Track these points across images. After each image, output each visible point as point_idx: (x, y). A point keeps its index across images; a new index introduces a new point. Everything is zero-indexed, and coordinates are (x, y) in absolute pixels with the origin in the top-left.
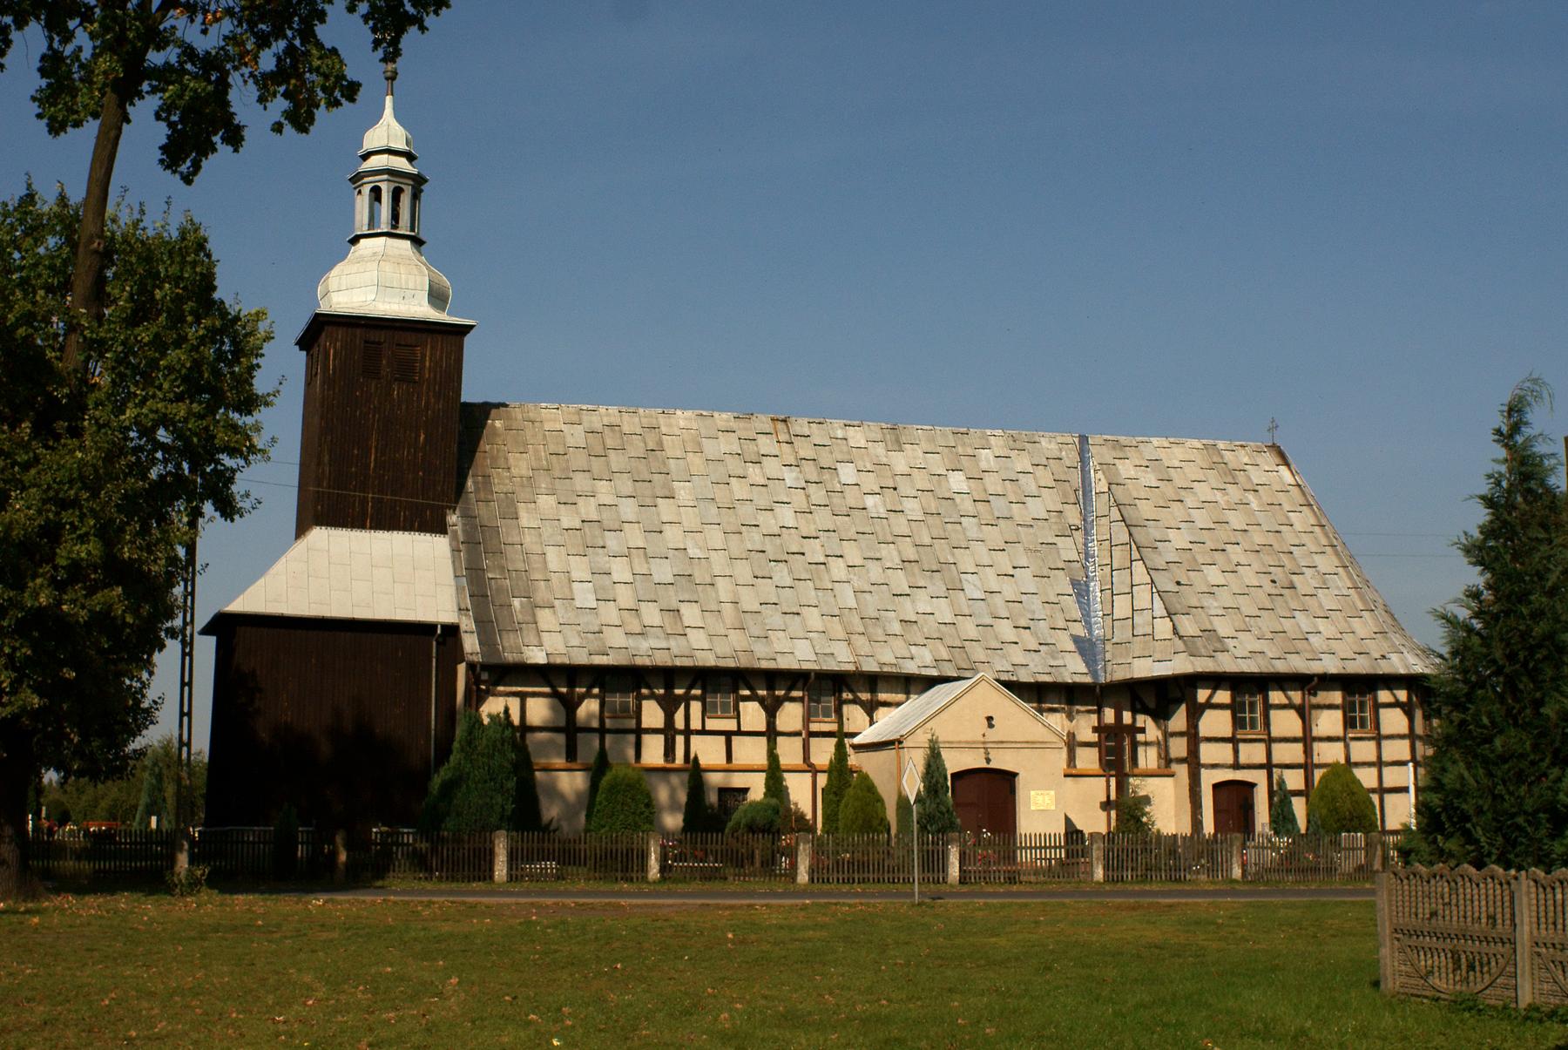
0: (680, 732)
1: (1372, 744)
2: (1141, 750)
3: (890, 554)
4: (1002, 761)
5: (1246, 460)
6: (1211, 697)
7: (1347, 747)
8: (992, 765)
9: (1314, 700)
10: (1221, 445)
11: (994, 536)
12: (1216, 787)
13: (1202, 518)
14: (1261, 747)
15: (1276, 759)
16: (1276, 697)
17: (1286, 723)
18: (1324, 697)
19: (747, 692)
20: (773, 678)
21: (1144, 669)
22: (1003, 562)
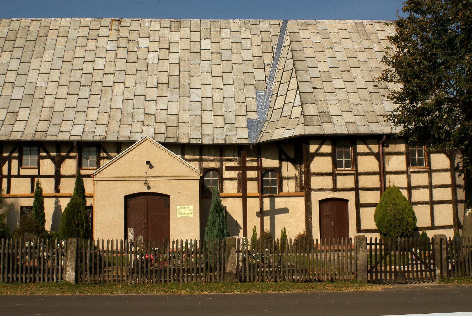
0: (5, 177)
1: (426, 175)
2: (285, 182)
3: (152, 81)
4: (158, 187)
5: (378, 28)
6: (318, 149)
7: (409, 177)
8: (152, 190)
9: (386, 150)
10: (365, 22)
11: (217, 70)
12: (321, 202)
13: (340, 56)
14: (352, 178)
15: (427, 191)
16: (361, 148)
17: (368, 163)
18: (392, 148)
19: (44, 154)
20: (59, 145)
21: (279, 134)
22: (218, 83)
